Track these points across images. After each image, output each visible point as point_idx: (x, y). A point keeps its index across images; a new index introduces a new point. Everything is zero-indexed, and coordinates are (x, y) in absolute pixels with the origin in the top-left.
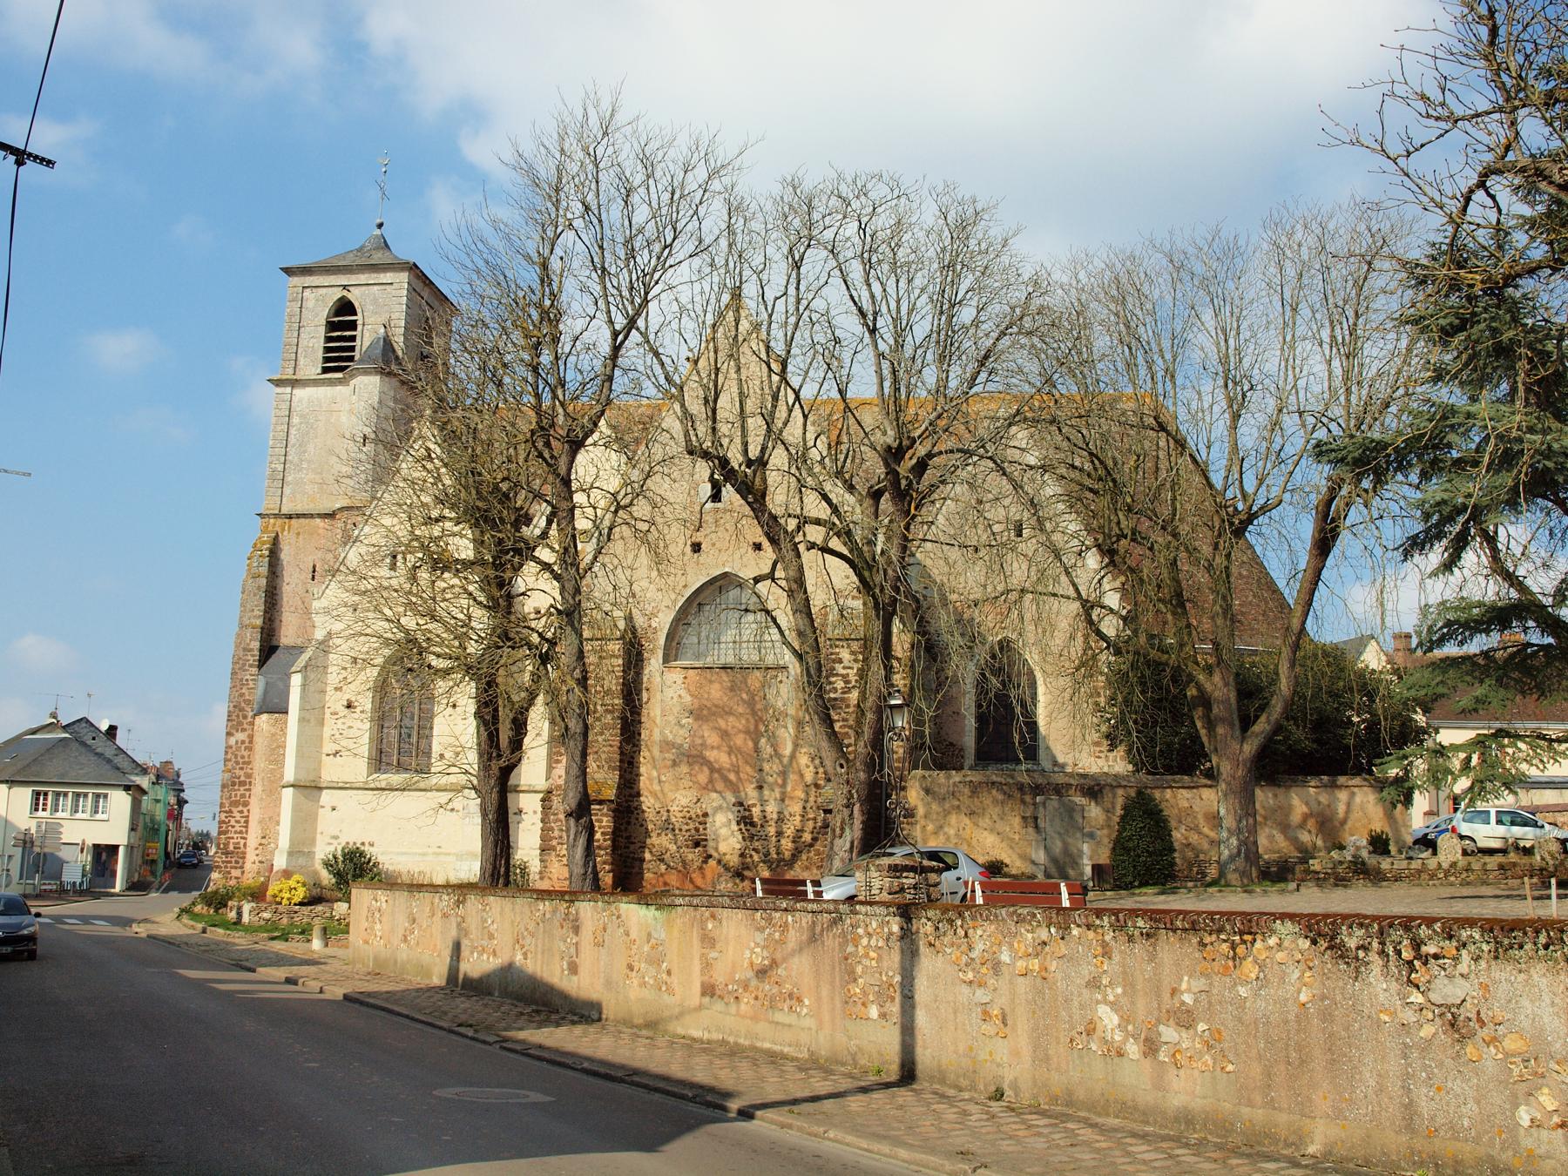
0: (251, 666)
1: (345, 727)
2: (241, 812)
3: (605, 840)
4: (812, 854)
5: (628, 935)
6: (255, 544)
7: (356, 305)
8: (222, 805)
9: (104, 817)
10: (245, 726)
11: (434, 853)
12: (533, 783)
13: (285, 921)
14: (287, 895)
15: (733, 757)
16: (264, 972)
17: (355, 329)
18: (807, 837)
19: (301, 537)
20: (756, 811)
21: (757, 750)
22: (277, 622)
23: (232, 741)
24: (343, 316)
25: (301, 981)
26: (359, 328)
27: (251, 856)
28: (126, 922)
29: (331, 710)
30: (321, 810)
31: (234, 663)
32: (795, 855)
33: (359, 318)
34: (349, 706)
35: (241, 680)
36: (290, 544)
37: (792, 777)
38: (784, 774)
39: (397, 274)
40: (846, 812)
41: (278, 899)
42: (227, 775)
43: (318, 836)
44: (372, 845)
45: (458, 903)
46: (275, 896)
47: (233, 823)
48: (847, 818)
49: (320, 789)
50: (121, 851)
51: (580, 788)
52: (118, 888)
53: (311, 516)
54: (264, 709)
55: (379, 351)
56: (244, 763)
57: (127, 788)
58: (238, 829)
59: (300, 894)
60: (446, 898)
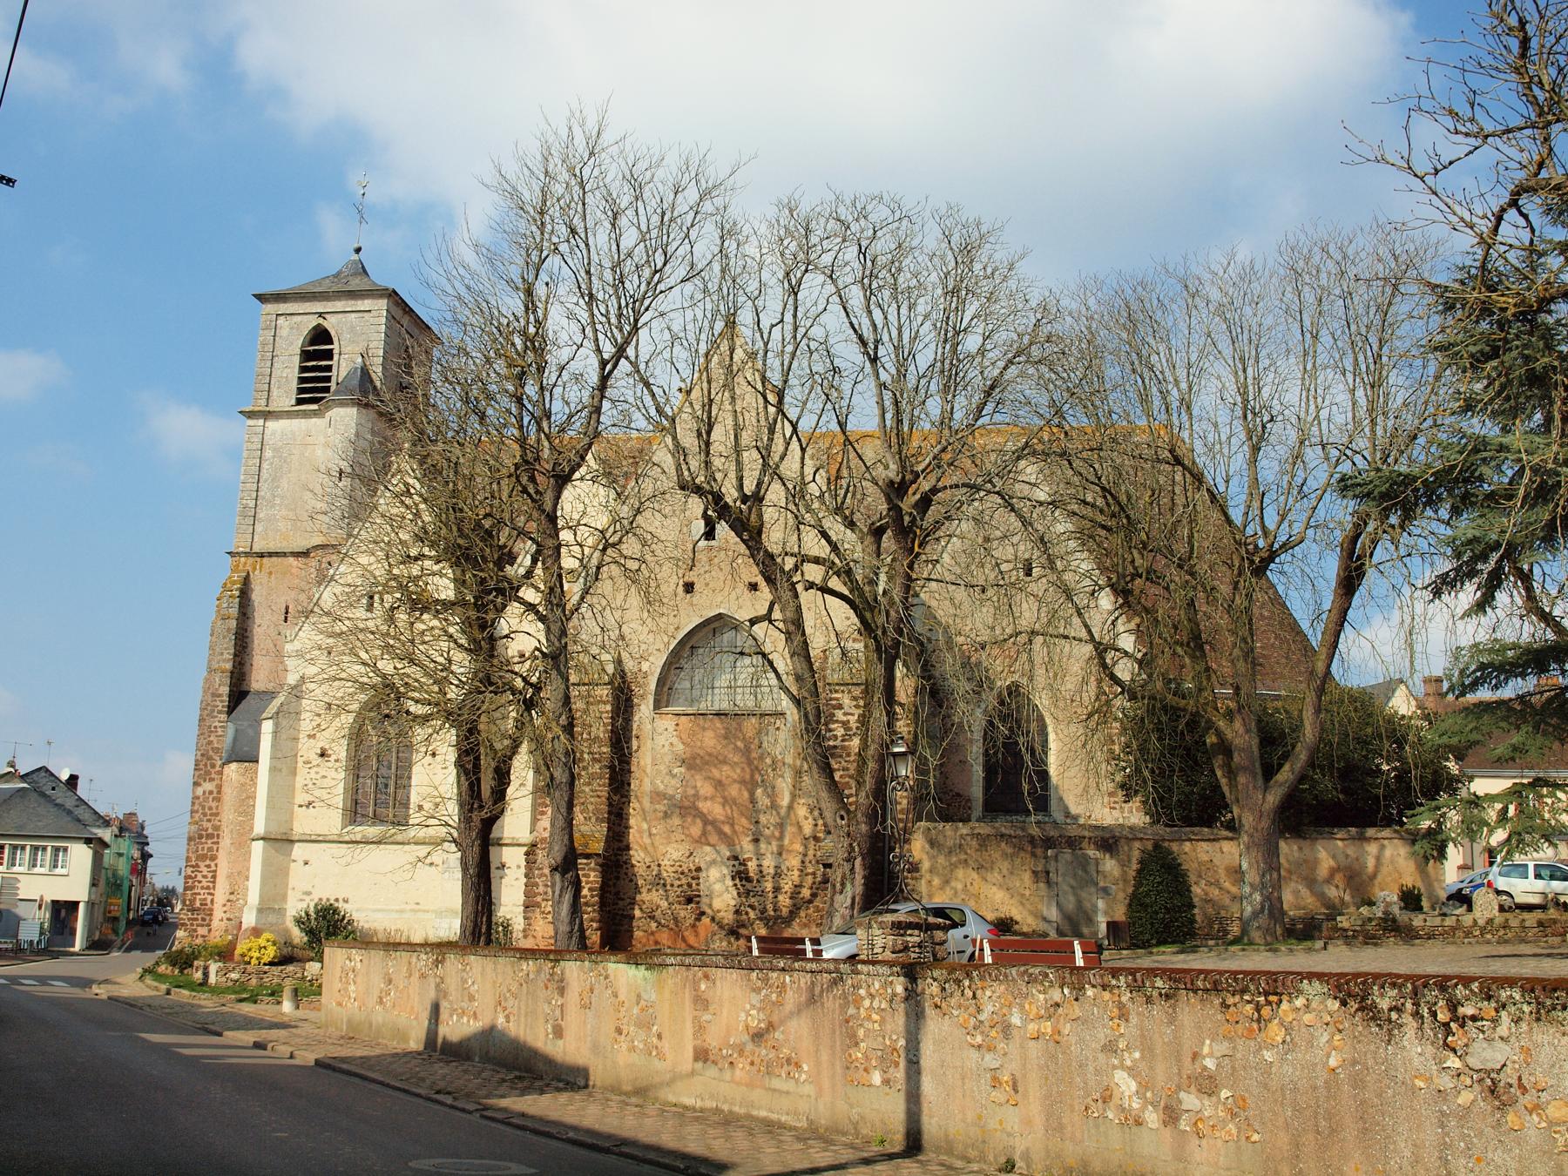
0: (220, 712)
1: (318, 777)
2: (209, 866)
3: (592, 896)
6: (225, 584)
7: (333, 333)
8: (188, 859)
9: (64, 871)
11: (412, 910)
12: (517, 836)
13: (254, 981)
14: (256, 954)
15: (727, 808)
17: (331, 358)
18: (806, 893)
20: (752, 866)
21: (753, 801)
23: (199, 791)
24: (319, 344)
26: (336, 357)
27: (218, 913)
28: (86, 983)
30: (292, 864)
31: (202, 709)
32: (794, 913)
33: (335, 346)
34: (322, 755)
37: (790, 830)
38: (781, 826)
39: (376, 301)
40: (847, 866)
41: (247, 959)
43: (290, 892)
44: (346, 901)
45: (437, 963)
46: (243, 955)
47: (199, 877)
48: (848, 873)
49: (292, 842)
50: (82, 907)
51: (566, 841)
52: (77, 948)
53: (284, 554)
54: (234, 757)
55: (356, 382)
56: (211, 815)
57: (88, 841)
58: (205, 884)
59: (271, 952)
60: (424, 957)
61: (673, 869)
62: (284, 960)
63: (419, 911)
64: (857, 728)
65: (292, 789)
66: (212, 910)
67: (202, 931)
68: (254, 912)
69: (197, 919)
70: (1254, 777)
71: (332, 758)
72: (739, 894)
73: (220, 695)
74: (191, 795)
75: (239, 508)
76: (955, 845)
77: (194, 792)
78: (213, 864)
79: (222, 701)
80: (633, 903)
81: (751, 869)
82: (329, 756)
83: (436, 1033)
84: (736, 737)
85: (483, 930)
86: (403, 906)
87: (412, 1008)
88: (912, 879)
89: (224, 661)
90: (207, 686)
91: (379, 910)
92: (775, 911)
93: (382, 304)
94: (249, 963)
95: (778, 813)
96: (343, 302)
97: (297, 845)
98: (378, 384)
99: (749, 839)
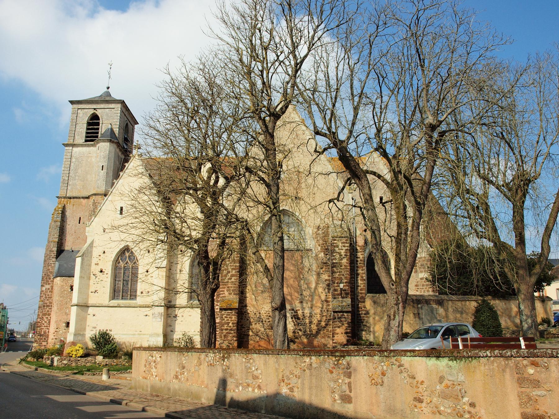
0: (53, 258)
1: (99, 280)
2: (47, 318)
3: (234, 326)
4: (325, 331)
5: (413, 378)
6: (55, 209)
7: (100, 116)
8: (38, 315)
10: (50, 282)
11: (138, 334)
13: (74, 364)
14: (75, 353)
15: (289, 288)
16: (92, 396)
17: (99, 125)
18: (323, 324)
20: (300, 313)
21: (300, 286)
22: (64, 240)
23: (44, 289)
24: (94, 121)
25: (124, 402)
26: (101, 125)
27: (51, 336)
29: (94, 273)
30: (88, 316)
31: (45, 257)
32: (318, 332)
33: (101, 122)
34: (101, 271)
35: (49, 263)
36: (70, 209)
37: (316, 297)
38: (312, 296)
39: (116, 105)
40: (396, 307)
41: (71, 355)
42: (41, 303)
43: (87, 327)
44: (111, 331)
45: (223, 358)
46: (69, 354)
47: (43, 322)
48: (396, 310)
49: (88, 307)
51: (282, 295)
53: (79, 198)
54: (59, 275)
55: (109, 133)
56: (49, 298)
58: (45, 325)
59: (81, 352)
60: (212, 355)
61: (266, 315)
62: (86, 355)
63: (141, 334)
64: (345, 255)
65: (88, 285)
66: (48, 335)
67: (44, 343)
68: (73, 336)
69: (42, 339)
70: (526, 271)
71: (105, 273)
72: (295, 325)
73: (53, 251)
74: (40, 290)
75: (61, 180)
76: (384, 303)
77: (41, 289)
78: (49, 317)
79: (54, 253)
80: (249, 329)
81: (299, 314)
82: (104, 272)
83: (225, 396)
84: (292, 259)
85: (213, 341)
86: (135, 333)
87: (203, 382)
88: (366, 317)
89: (55, 238)
90: (48, 247)
92: (310, 331)
93: (119, 106)
94: (72, 357)
95: (310, 291)
98: (117, 135)
99: (298, 302)
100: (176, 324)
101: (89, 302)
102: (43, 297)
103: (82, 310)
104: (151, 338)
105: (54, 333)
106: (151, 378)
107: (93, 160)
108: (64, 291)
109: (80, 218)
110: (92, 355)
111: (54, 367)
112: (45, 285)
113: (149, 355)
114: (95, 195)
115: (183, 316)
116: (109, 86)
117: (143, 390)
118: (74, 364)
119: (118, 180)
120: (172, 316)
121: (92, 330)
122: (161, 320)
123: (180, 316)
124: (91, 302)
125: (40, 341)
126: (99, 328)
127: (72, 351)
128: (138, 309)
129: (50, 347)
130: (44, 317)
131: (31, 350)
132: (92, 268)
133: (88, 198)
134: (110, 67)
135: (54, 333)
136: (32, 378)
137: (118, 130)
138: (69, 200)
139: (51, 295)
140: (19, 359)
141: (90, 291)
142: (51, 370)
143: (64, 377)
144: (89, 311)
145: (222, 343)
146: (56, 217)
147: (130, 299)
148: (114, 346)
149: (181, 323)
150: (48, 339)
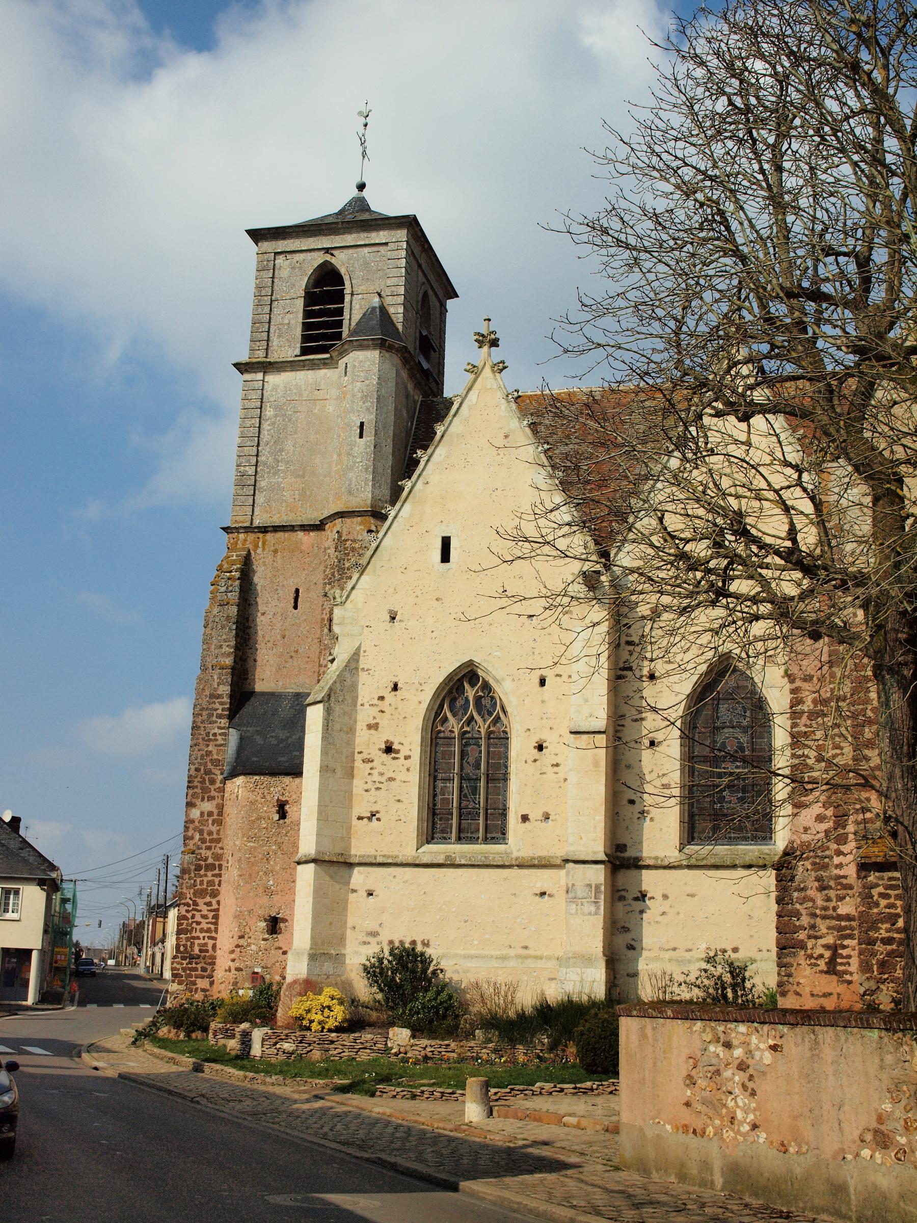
0: (220, 716)
1: (383, 779)
6: (221, 567)
7: (343, 271)
9: (15, 916)
10: (213, 793)
11: (519, 957)
12: (661, 854)
13: (316, 1055)
14: (318, 1017)
19: (279, 554)
22: (251, 662)
23: (195, 813)
26: (347, 298)
27: (223, 961)
28: (71, 1050)
29: (365, 756)
30: (352, 897)
34: (389, 750)
35: (208, 734)
36: (264, 564)
39: (393, 232)
43: (349, 932)
46: (300, 1018)
47: (198, 918)
49: (351, 865)
50: (35, 956)
52: (30, 1001)
53: (291, 528)
56: (211, 841)
57: (41, 883)
58: (204, 926)
59: (339, 1014)
62: (353, 1025)
65: (349, 795)
67: (202, 983)
69: (196, 969)
73: (219, 696)
74: (184, 818)
77: (187, 815)
79: (222, 703)
82: (398, 752)
90: (202, 681)
91: (472, 957)
93: (402, 235)
94: (309, 1029)
96: (354, 235)
97: (357, 870)
98: (400, 327)
100: (644, 924)
101: (353, 852)
102: (192, 838)
103: (331, 877)
104: (564, 970)
105: (232, 952)
106: (728, 1134)
107: (330, 409)
108: (259, 818)
109: (297, 591)
110: (371, 1025)
111: (253, 1060)
112: (198, 802)
113: (708, 1037)
114: (341, 515)
115: (665, 897)
116: (364, 180)
117: (683, 1177)
118: (316, 1055)
119: (429, 451)
120: (630, 896)
121: (365, 943)
122: (598, 908)
123: (659, 896)
124: (359, 849)
125: (190, 976)
126: (385, 936)
127: (308, 1011)
128: (515, 871)
129: (221, 996)
130: (201, 902)
131: (164, 1002)
132: (358, 741)
133: (319, 527)
134: (363, 120)
135: (232, 952)
136: (204, 1101)
137: (401, 310)
138: (261, 535)
139: (218, 832)
140: (133, 1032)
141: (356, 812)
142: (251, 1075)
143: (308, 1101)
144: (353, 880)
145: (873, 992)
146: (223, 589)
147: (486, 840)
148: (444, 996)
149: (659, 918)
150: (213, 970)
